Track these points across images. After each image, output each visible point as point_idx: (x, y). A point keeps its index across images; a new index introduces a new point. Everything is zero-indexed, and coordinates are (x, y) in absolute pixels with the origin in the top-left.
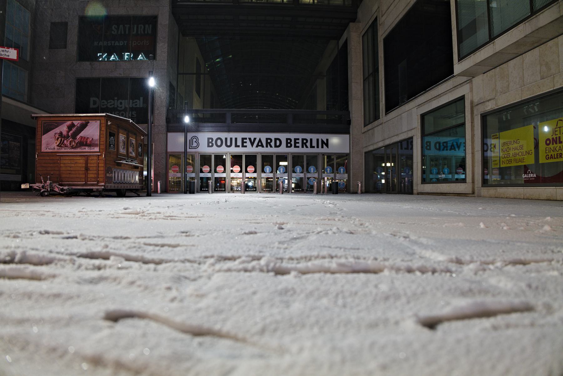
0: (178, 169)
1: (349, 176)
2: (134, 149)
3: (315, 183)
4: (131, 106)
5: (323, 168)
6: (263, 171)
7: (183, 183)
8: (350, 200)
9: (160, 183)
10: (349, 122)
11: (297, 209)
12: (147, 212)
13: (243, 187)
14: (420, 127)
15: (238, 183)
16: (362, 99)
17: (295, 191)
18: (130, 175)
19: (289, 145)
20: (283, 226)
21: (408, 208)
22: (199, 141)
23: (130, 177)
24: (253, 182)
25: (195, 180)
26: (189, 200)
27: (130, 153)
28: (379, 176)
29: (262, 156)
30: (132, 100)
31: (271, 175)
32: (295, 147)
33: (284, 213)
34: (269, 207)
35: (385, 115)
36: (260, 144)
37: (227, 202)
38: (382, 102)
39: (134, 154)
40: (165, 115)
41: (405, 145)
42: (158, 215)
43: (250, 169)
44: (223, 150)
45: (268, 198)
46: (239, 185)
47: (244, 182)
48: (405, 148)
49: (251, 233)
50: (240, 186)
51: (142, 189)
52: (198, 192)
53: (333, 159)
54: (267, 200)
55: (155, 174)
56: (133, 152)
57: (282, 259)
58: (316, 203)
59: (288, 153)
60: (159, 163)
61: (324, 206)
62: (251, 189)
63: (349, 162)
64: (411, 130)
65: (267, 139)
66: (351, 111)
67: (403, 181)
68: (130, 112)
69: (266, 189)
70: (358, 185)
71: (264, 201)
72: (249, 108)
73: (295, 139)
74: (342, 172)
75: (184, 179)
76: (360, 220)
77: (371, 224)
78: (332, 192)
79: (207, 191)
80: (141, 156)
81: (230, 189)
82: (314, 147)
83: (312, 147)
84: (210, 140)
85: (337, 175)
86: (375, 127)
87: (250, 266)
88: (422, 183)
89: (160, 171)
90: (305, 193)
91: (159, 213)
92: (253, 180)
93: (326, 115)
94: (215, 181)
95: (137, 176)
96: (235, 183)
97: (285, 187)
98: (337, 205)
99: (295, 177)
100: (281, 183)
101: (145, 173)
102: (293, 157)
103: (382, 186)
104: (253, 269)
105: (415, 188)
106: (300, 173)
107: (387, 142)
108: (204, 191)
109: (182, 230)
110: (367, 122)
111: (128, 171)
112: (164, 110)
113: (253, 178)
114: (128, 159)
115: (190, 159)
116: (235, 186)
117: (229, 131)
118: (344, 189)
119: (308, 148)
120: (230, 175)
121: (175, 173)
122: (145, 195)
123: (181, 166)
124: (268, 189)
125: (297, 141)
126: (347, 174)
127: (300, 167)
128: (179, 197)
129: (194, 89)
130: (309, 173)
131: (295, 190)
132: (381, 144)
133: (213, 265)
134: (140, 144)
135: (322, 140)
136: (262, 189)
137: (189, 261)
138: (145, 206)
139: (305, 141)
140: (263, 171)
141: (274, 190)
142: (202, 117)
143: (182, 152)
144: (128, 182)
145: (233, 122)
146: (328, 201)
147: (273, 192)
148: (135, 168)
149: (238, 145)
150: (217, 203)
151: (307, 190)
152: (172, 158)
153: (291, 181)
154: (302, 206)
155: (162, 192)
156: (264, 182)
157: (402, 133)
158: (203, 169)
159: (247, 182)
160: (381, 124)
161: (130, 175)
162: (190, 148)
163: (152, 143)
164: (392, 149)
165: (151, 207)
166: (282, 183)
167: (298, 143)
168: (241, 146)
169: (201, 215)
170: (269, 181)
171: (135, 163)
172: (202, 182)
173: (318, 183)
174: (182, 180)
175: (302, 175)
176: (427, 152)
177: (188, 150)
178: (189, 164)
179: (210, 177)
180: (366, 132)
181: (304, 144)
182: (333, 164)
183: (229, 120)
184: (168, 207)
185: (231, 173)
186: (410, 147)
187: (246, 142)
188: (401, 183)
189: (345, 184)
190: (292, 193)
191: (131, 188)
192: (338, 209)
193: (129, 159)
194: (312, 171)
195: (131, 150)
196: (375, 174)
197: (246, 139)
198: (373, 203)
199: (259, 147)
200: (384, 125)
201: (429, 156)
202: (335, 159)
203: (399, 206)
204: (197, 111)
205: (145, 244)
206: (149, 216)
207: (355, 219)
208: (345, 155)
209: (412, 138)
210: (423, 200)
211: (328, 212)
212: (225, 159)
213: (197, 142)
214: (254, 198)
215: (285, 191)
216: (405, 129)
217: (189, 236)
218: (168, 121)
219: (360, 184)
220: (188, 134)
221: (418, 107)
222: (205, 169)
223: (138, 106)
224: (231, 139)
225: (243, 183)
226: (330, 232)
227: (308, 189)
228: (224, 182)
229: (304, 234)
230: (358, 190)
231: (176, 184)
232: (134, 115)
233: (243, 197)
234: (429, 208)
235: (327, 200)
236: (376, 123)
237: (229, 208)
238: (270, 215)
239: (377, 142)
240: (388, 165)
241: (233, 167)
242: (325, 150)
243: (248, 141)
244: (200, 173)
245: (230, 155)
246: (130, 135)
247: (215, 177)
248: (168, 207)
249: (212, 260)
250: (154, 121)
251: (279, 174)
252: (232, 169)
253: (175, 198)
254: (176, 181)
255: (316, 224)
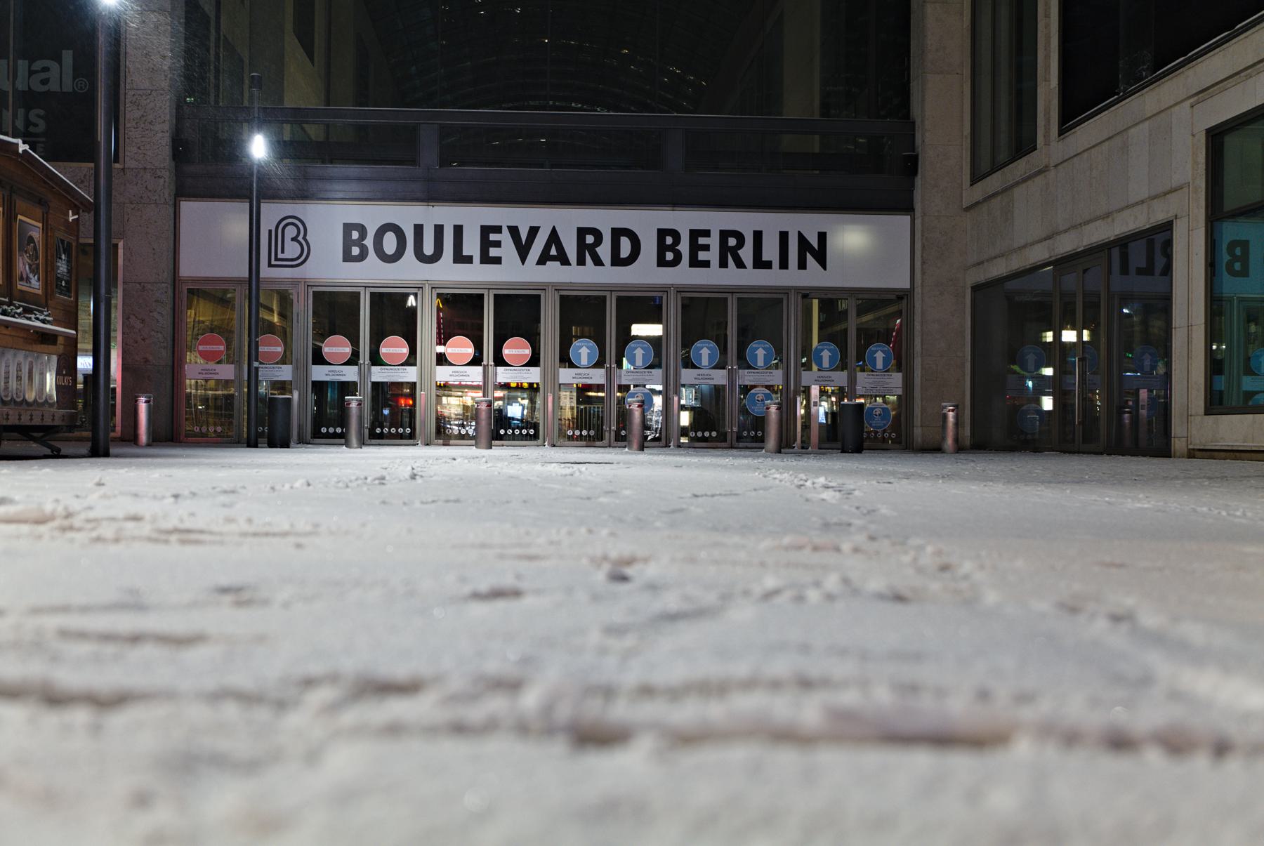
0: (222, 348)
1: (908, 385)
2: (38, 265)
3: (773, 409)
4: (21, 86)
5: (806, 350)
6: (566, 360)
7: (241, 408)
8: (907, 476)
9: (146, 402)
10: (911, 166)
11: (692, 508)
12: (83, 516)
13: (484, 423)
14: (1201, 183)
15: (468, 407)
16: (967, 71)
17: (692, 439)
18: (19, 370)
19: (669, 256)
20: (629, 571)
21: (1141, 509)
22: (308, 238)
23: (19, 378)
24: (526, 402)
25: (291, 393)
26: (264, 472)
27: (21, 279)
28: (1030, 384)
29: (562, 297)
30: (27, 62)
31: (598, 376)
32: (695, 263)
33: (641, 523)
34: (581, 498)
35: (1060, 135)
36: (553, 252)
37: (419, 480)
38: (1047, 80)
39: (36, 285)
40: (166, 127)
41: (1138, 256)
42: (130, 525)
43: (514, 351)
44: (407, 271)
45: (583, 467)
46: (470, 414)
47: (490, 404)
48: (1138, 268)
49: (497, 594)
50: (472, 418)
51: (71, 427)
52: (302, 441)
53: (845, 312)
54: (577, 474)
55: (125, 368)
56: (31, 276)
57: (609, 692)
58: (771, 487)
59: (665, 289)
60: (143, 321)
61: (801, 496)
62: (517, 432)
63: (909, 323)
64: (1166, 194)
65: (582, 232)
66: (918, 123)
67: (1130, 403)
68: (21, 112)
69: (577, 433)
70: (945, 417)
71: (566, 475)
72: (511, 105)
73: (695, 234)
74: (880, 365)
75: (246, 390)
76: (939, 553)
77: (982, 567)
78: (839, 445)
79: (341, 438)
80: (68, 290)
81: (434, 430)
82: (768, 265)
83: (760, 263)
84: (355, 235)
85: (861, 377)
86: (1017, 184)
87: (476, 713)
88: (1208, 411)
89: (150, 358)
90: (732, 447)
91: (136, 518)
92: (525, 396)
93: (817, 137)
94: (374, 399)
95: (48, 375)
96: (452, 405)
97: (653, 423)
98: (857, 493)
99: (692, 386)
100: (635, 407)
101: (85, 363)
102: (684, 307)
103: (1041, 420)
104: (489, 727)
105: (1177, 428)
106: (715, 368)
107: (1067, 245)
108: (328, 436)
109: (224, 581)
110: (985, 165)
111: (12, 351)
112: (163, 109)
113: (526, 385)
114: (10, 304)
115: (271, 310)
116: (456, 419)
117: (431, 197)
118: (886, 435)
119: (744, 267)
120: (432, 374)
121: (212, 365)
122: (85, 451)
123: (236, 337)
124: (585, 433)
125: (702, 241)
126: (900, 375)
127: (713, 344)
128: (238, 461)
129: (289, 26)
130: (750, 367)
131: (692, 434)
132: (1038, 254)
133: (333, 708)
134: (62, 241)
135: (801, 237)
136: (560, 430)
137: (247, 698)
138: (79, 494)
139: (732, 242)
140: (566, 360)
141: (607, 434)
142: (321, 138)
143: (238, 281)
144: (12, 399)
145: (444, 162)
146: (822, 480)
147: (606, 442)
148: (42, 343)
149: (465, 253)
150: (377, 482)
151: (739, 438)
152: (198, 300)
153: (676, 399)
154: (713, 496)
155: (153, 441)
156: (568, 401)
157: (1128, 207)
158: (326, 350)
159: (500, 403)
160: (1040, 172)
161: (19, 370)
162: (273, 262)
163: (114, 241)
164: (1085, 271)
165: (105, 497)
166: (639, 406)
167: (706, 248)
168: (477, 258)
169: (308, 528)
170: (590, 400)
171: (43, 321)
172: (320, 402)
173: (784, 409)
174: (240, 391)
175: (720, 377)
176: (1231, 286)
177: (266, 272)
178: (270, 328)
179: (355, 383)
180: (977, 203)
181: (729, 254)
182: (846, 331)
183: (429, 154)
184: (176, 496)
185: (439, 368)
186: (1160, 262)
187: (498, 244)
188: (1120, 413)
189: (893, 413)
190: (680, 446)
191: (25, 420)
192: (858, 508)
193: (14, 305)
194: (760, 362)
195: (22, 265)
196: (1015, 372)
197: (498, 229)
198: (1000, 487)
199: (548, 263)
200: (1052, 174)
201: (1241, 300)
202: (852, 314)
203: (1109, 503)
204: (298, 116)
205: (64, 634)
206: (93, 529)
207: (920, 548)
208: (893, 297)
209: (1167, 227)
210: (1210, 478)
211: (814, 519)
212: (413, 311)
213: (302, 239)
214: (524, 466)
215: (651, 440)
216: (1139, 190)
217: (248, 603)
218: (180, 150)
219: (951, 415)
220: (265, 207)
221: (1196, 98)
222: (335, 350)
223: (54, 86)
224: (439, 230)
225: (483, 407)
226: (813, 595)
227: (745, 434)
228: (411, 402)
229: (710, 598)
230: (944, 438)
231: (215, 409)
232: (36, 125)
233: (484, 460)
234: (1232, 512)
235: (817, 477)
236: (1021, 167)
237: (422, 503)
238: (583, 530)
239: (1024, 247)
240: (1069, 336)
241: (445, 344)
242: (813, 276)
243: (505, 237)
244: (314, 363)
245: (435, 296)
246: (20, 204)
247: (373, 380)
248: (176, 496)
249: (323, 695)
250: (121, 151)
251: (628, 371)
252: (440, 349)
253: (207, 464)
254: (216, 398)
255: (763, 564)
